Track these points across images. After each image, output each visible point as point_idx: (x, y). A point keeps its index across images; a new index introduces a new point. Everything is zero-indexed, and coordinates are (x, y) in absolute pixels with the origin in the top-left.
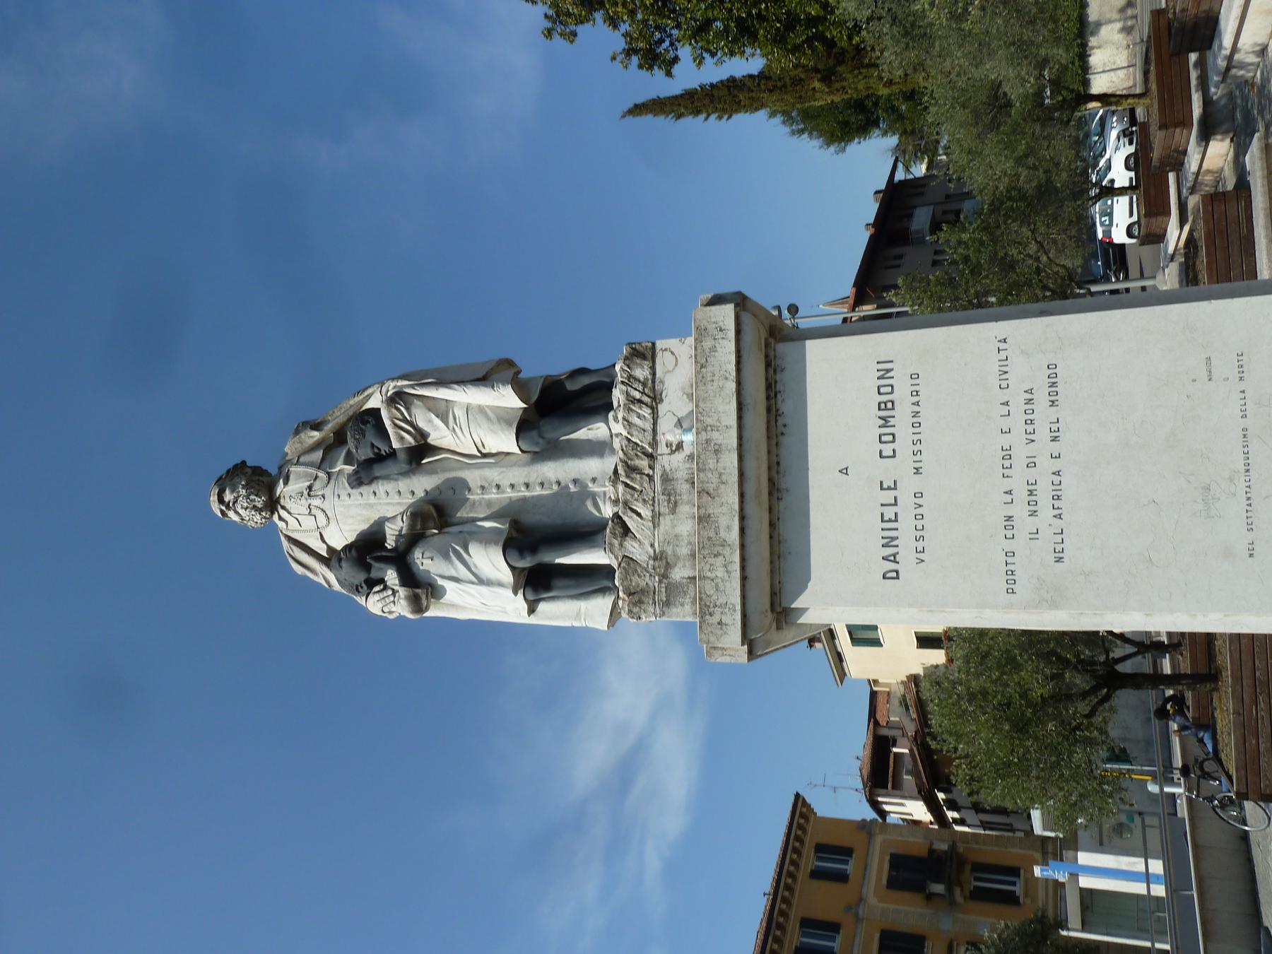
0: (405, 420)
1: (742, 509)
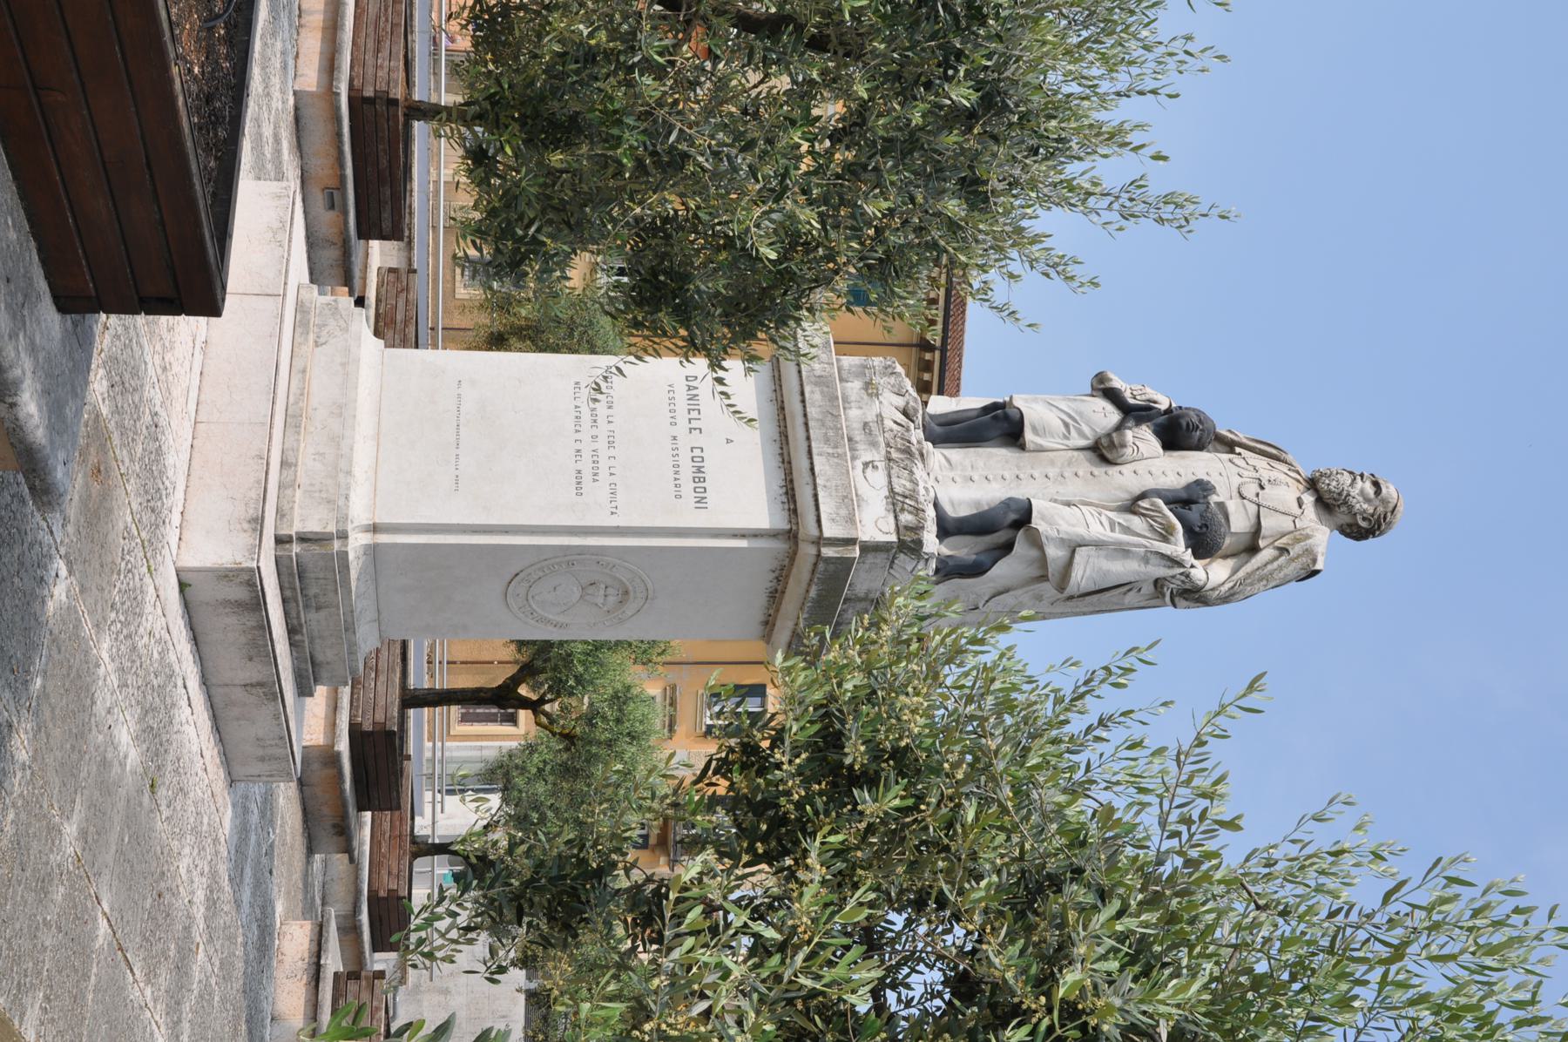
0: (1151, 517)
1: (805, 407)
